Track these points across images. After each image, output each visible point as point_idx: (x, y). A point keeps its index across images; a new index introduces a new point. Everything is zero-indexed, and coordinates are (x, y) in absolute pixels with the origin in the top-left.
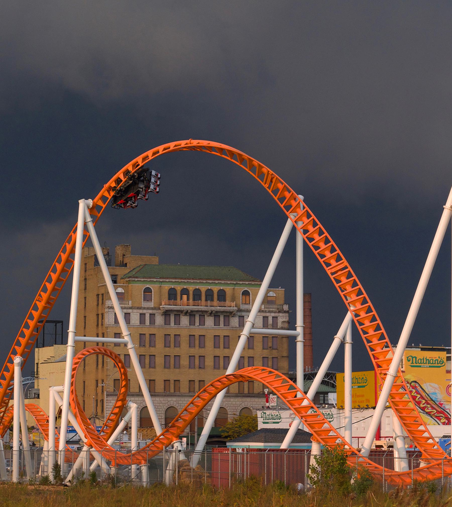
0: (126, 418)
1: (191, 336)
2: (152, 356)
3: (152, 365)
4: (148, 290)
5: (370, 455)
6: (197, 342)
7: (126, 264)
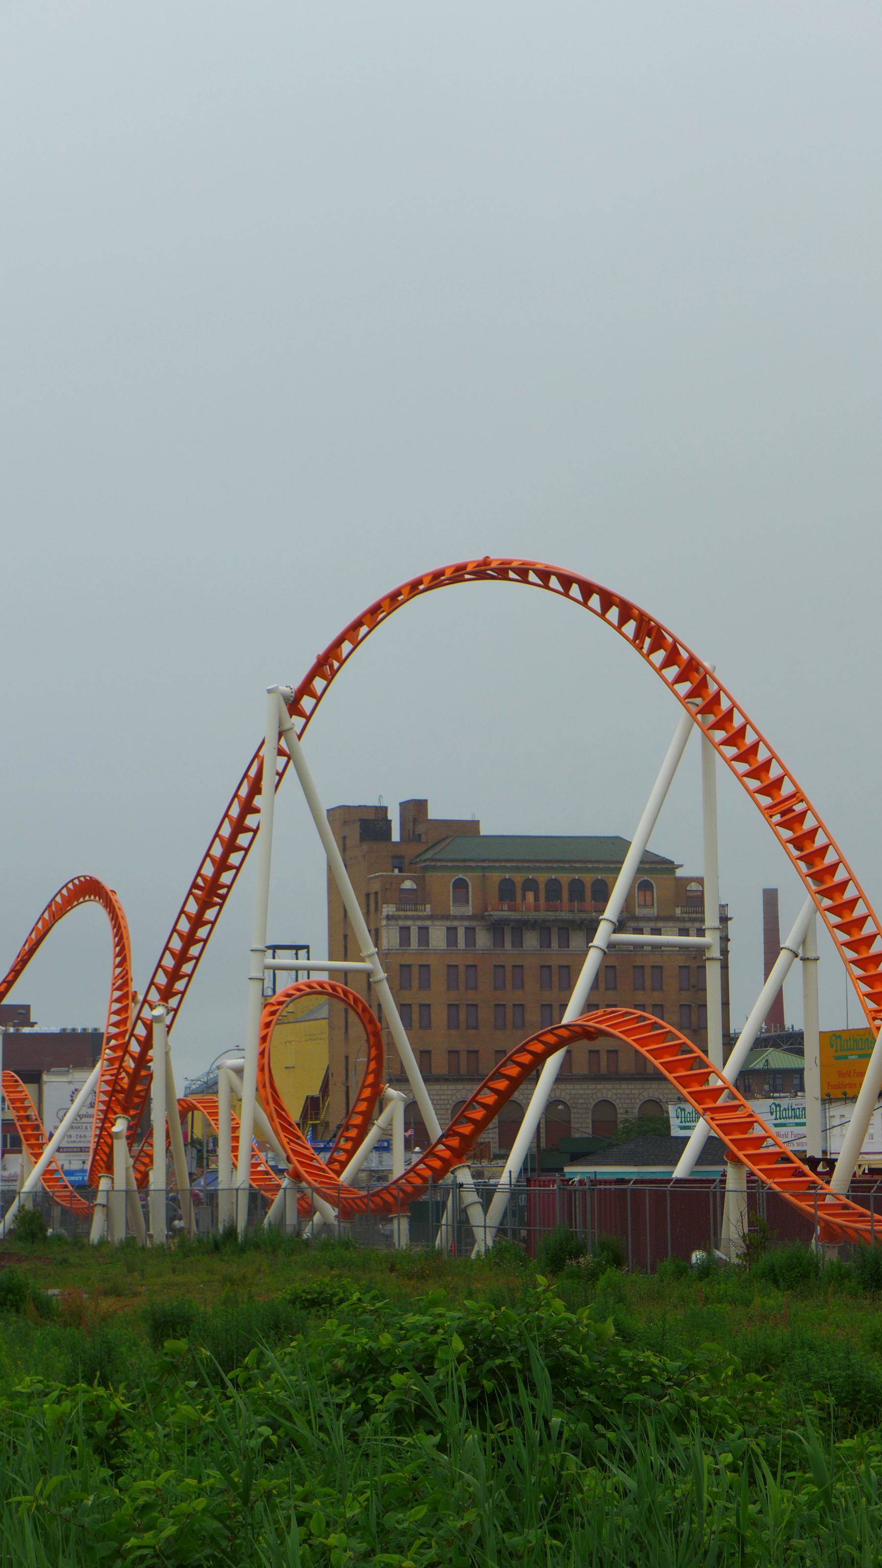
0: (381, 1121)
1: (452, 968)
2: (425, 1007)
3: (426, 1024)
4: (460, 885)
5: (853, 1189)
6: (555, 979)
7: (420, 835)
